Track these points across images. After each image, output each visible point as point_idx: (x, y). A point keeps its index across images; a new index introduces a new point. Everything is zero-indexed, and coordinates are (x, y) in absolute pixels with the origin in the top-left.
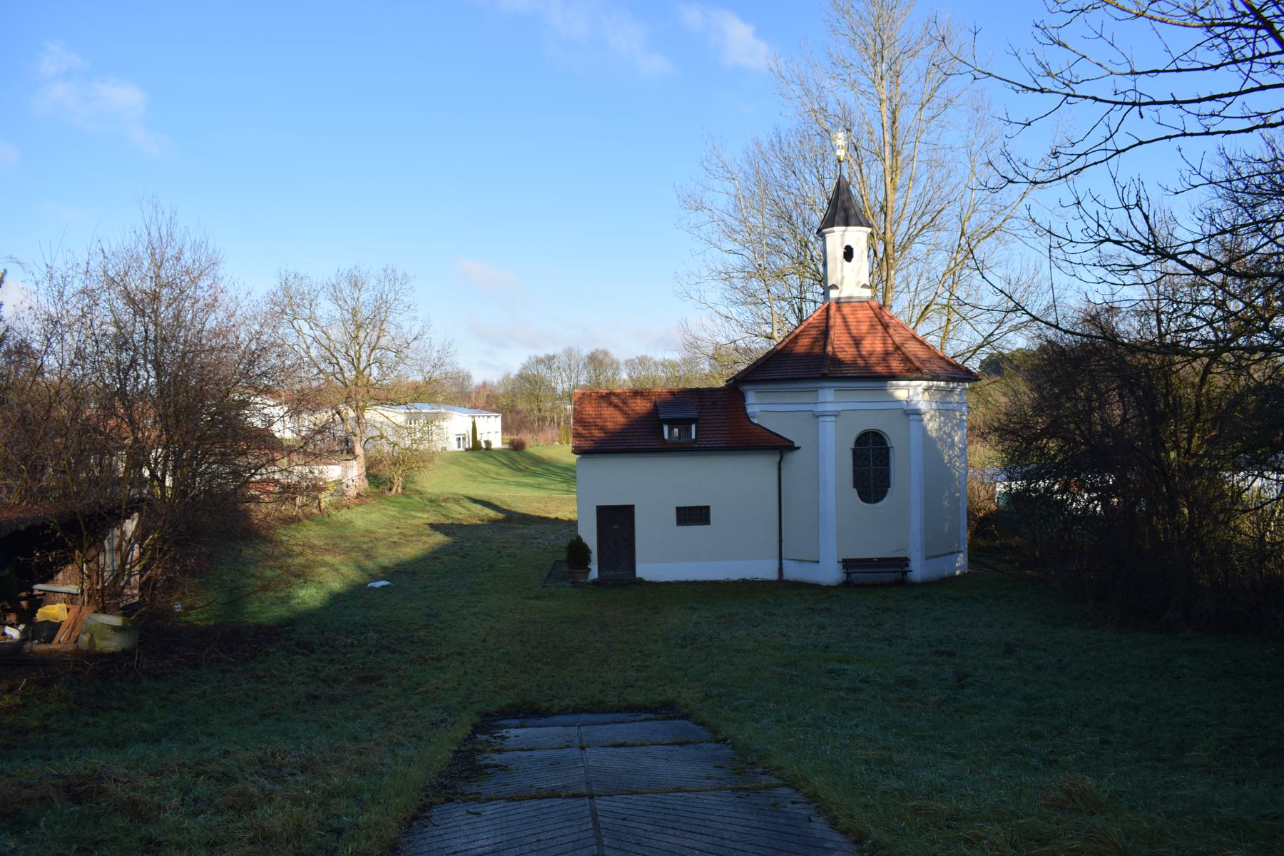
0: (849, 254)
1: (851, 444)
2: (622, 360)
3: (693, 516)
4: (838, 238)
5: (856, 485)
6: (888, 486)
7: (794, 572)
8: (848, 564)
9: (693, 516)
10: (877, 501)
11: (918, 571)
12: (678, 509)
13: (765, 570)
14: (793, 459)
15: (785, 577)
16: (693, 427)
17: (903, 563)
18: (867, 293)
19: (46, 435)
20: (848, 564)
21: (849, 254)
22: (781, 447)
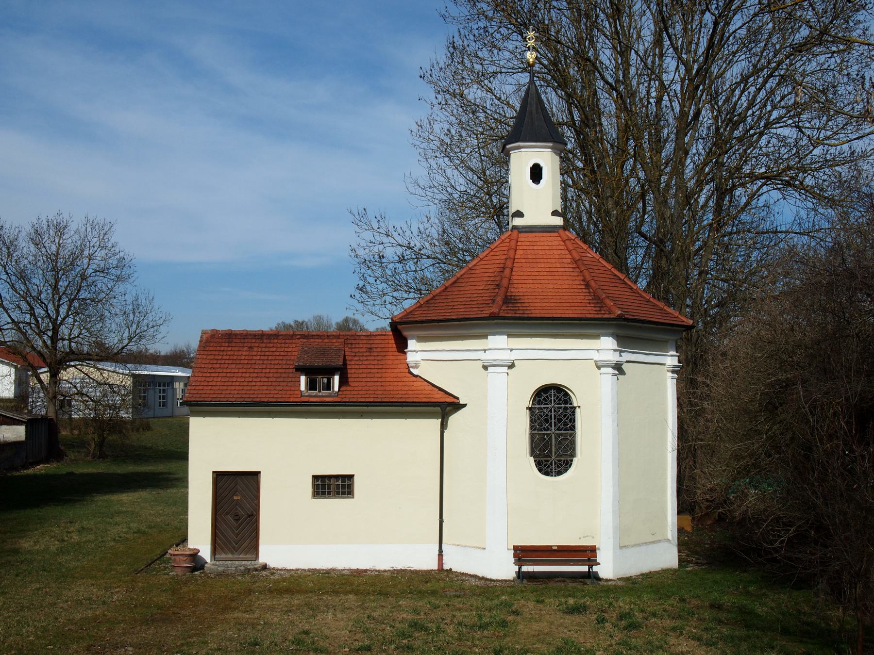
0: (536, 173)
1: (526, 400)
2: (516, 568)
3: (333, 486)
4: (522, 159)
5: (532, 453)
6: (573, 455)
7: (456, 562)
8: (523, 554)
9: (333, 486)
10: (559, 473)
11: (607, 568)
12: (315, 478)
13: (422, 559)
14: (455, 419)
15: (446, 567)
16: (337, 378)
17: (588, 554)
18: (559, 221)
19: (79, 603)
20: (523, 554)
21: (536, 173)
22: (445, 407)
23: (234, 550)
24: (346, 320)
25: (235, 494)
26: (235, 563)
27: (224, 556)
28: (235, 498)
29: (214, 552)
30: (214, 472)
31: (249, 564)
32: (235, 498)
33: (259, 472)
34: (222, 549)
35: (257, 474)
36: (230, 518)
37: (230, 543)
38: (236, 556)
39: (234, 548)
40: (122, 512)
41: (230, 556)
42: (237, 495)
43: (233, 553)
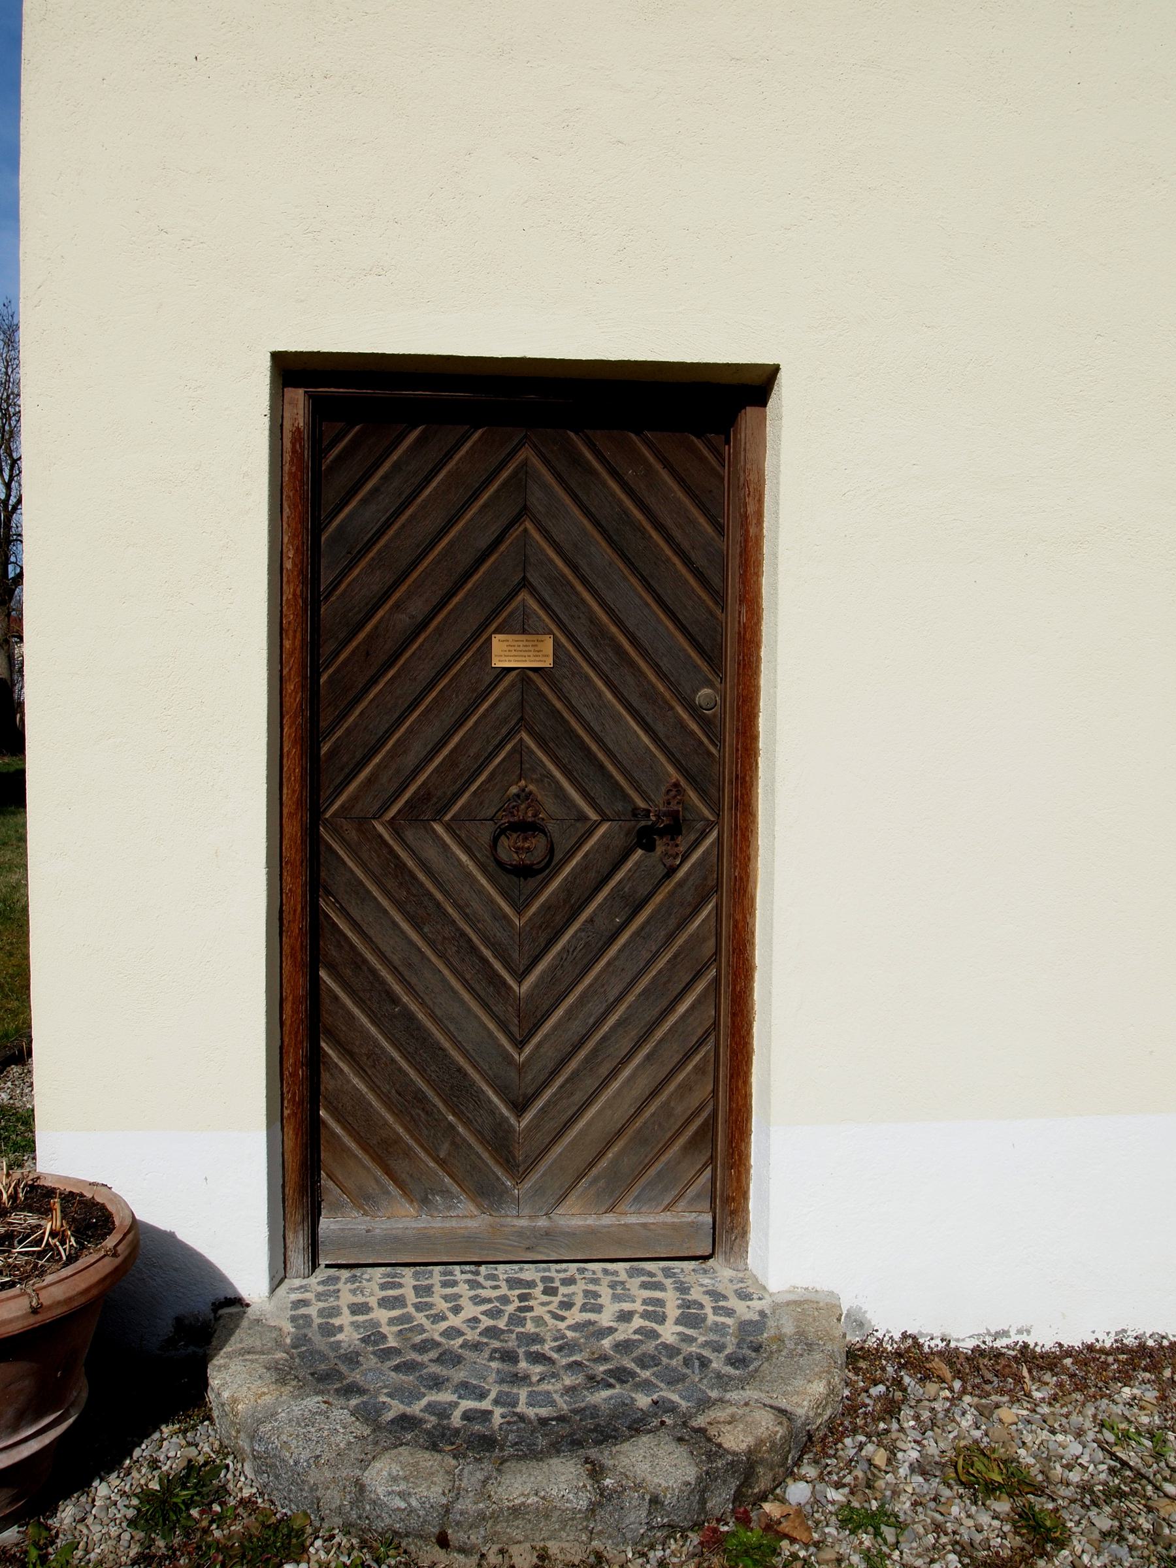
23: (497, 1160)
24: (237, 1302)
25: (501, 615)
26: (449, 1285)
27: (401, 1218)
28: (508, 652)
29: (302, 1186)
30: (290, 370)
31: (615, 1303)
32: (508, 652)
33: (751, 387)
34: (384, 1152)
35: (702, 418)
36: (452, 857)
37: (458, 1091)
38: (519, 1221)
39: (501, 1143)
40: (438, 1437)
41: (464, 1218)
42: (522, 626)
43: (487, 1193)
